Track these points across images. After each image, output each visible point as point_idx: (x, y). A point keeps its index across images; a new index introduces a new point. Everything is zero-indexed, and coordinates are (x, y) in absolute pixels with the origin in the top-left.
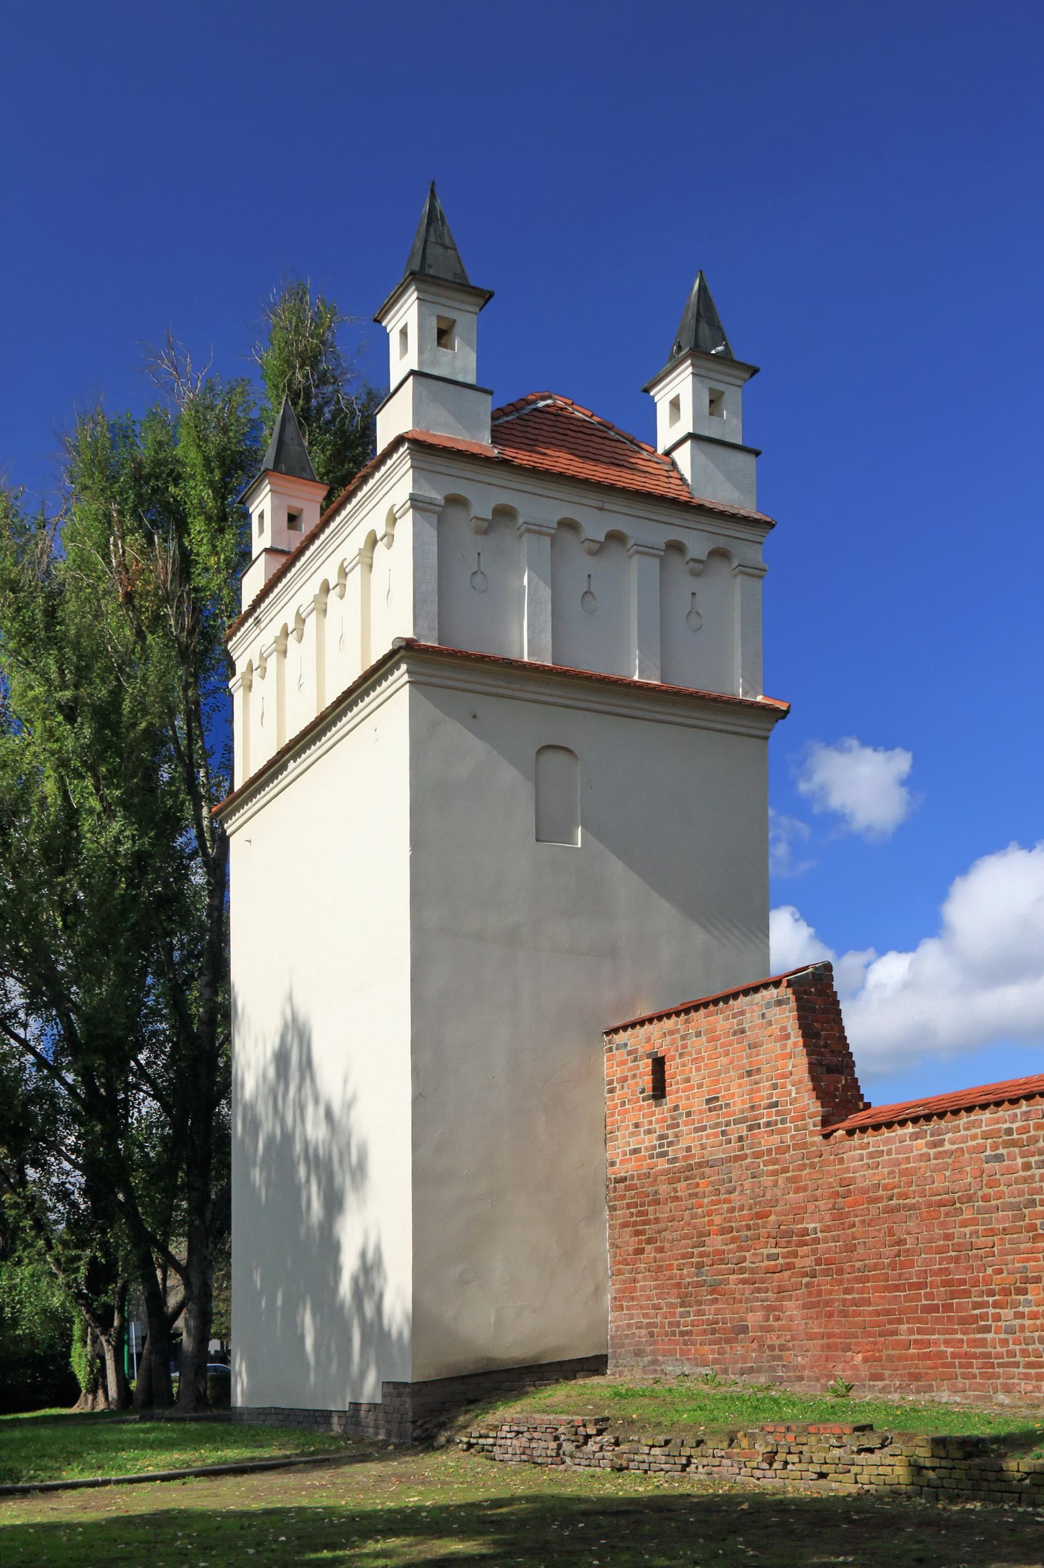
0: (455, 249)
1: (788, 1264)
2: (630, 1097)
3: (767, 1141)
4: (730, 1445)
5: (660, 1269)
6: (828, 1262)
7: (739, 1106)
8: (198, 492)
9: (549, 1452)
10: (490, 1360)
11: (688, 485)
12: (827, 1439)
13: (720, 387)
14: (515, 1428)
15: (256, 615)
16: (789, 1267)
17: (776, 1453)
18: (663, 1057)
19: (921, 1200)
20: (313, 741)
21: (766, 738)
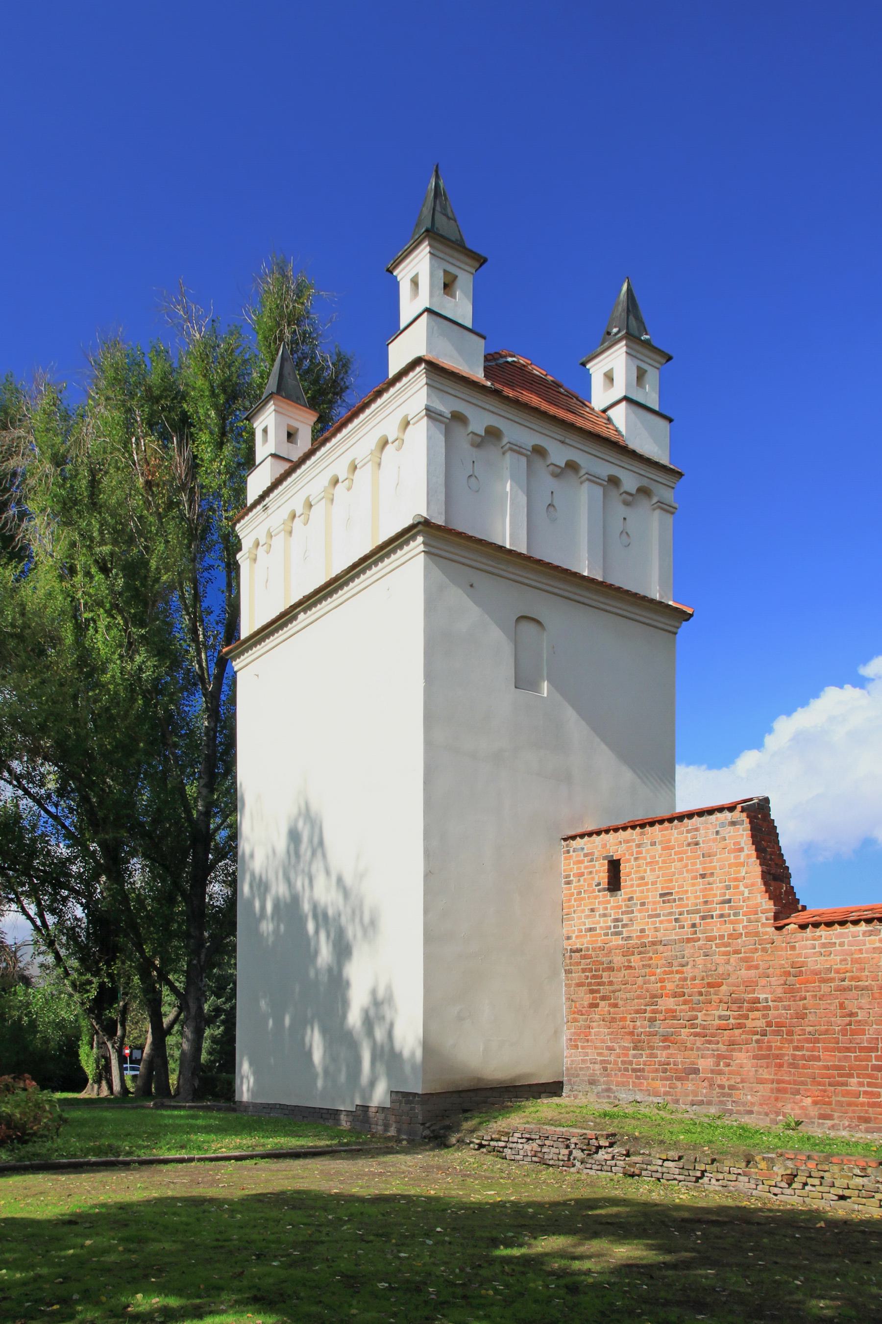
0: (456, 221)
1: (739, 1024)
2: (586, 888)
3: (717, 928)
4: (747, 1166)
5: (613, 1020)
6: (779, 1025)
7: (692, 901)
8: (206, 412)
9: (561, 1157)
10: (480, 1080)
11: (623, 436)
12: (851, 1169)
13: (645, 366)
14: (528, 1136)
15: (264, 503)
16: (740, 1026)
17: (796, 1176)
18: (619, 860)
19: (873, 983)
20: (325, 598)
21: (675, 633)
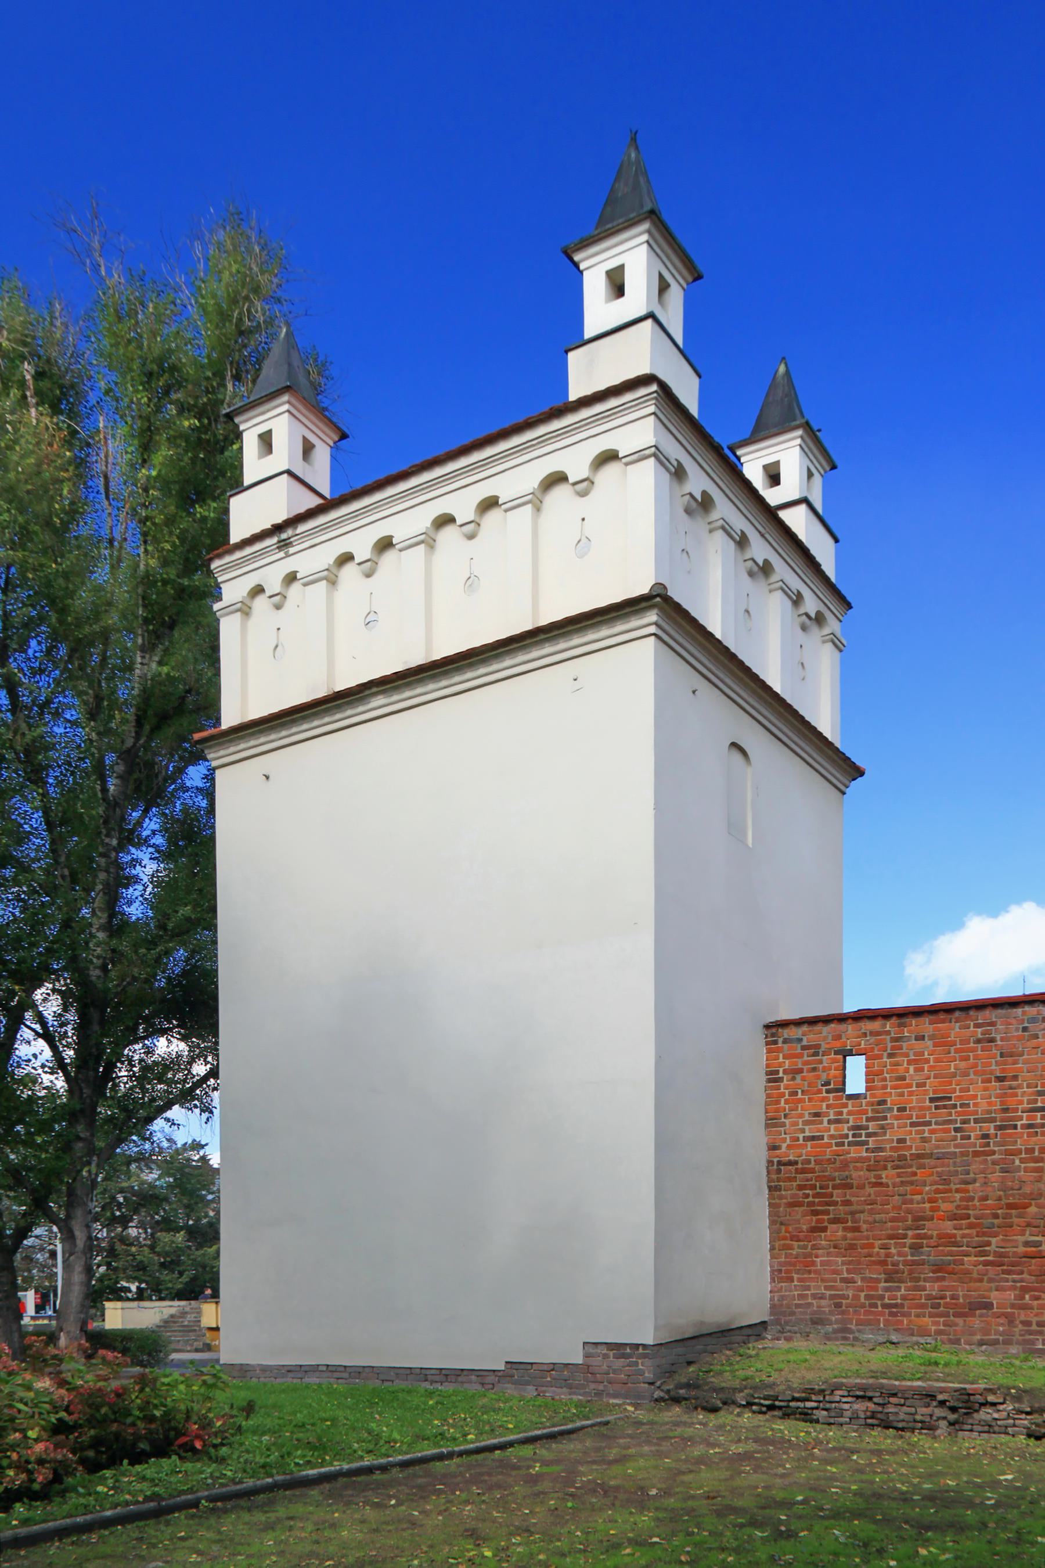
10: (702, 1323)
21: (844, 793)
